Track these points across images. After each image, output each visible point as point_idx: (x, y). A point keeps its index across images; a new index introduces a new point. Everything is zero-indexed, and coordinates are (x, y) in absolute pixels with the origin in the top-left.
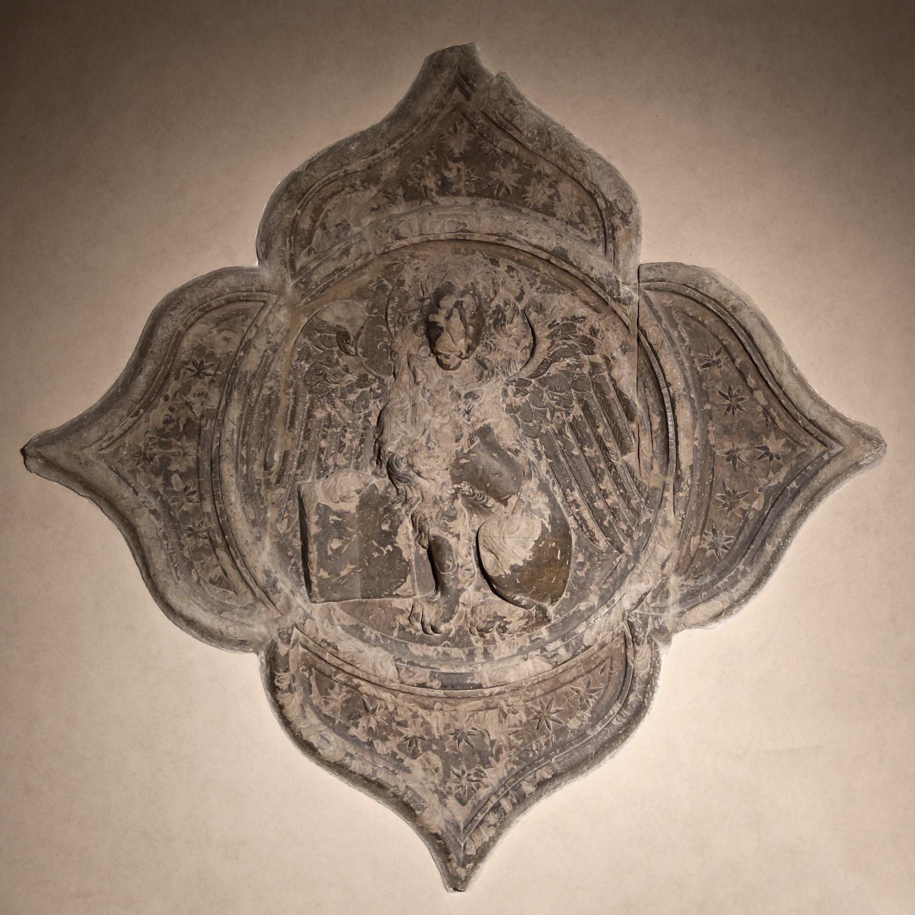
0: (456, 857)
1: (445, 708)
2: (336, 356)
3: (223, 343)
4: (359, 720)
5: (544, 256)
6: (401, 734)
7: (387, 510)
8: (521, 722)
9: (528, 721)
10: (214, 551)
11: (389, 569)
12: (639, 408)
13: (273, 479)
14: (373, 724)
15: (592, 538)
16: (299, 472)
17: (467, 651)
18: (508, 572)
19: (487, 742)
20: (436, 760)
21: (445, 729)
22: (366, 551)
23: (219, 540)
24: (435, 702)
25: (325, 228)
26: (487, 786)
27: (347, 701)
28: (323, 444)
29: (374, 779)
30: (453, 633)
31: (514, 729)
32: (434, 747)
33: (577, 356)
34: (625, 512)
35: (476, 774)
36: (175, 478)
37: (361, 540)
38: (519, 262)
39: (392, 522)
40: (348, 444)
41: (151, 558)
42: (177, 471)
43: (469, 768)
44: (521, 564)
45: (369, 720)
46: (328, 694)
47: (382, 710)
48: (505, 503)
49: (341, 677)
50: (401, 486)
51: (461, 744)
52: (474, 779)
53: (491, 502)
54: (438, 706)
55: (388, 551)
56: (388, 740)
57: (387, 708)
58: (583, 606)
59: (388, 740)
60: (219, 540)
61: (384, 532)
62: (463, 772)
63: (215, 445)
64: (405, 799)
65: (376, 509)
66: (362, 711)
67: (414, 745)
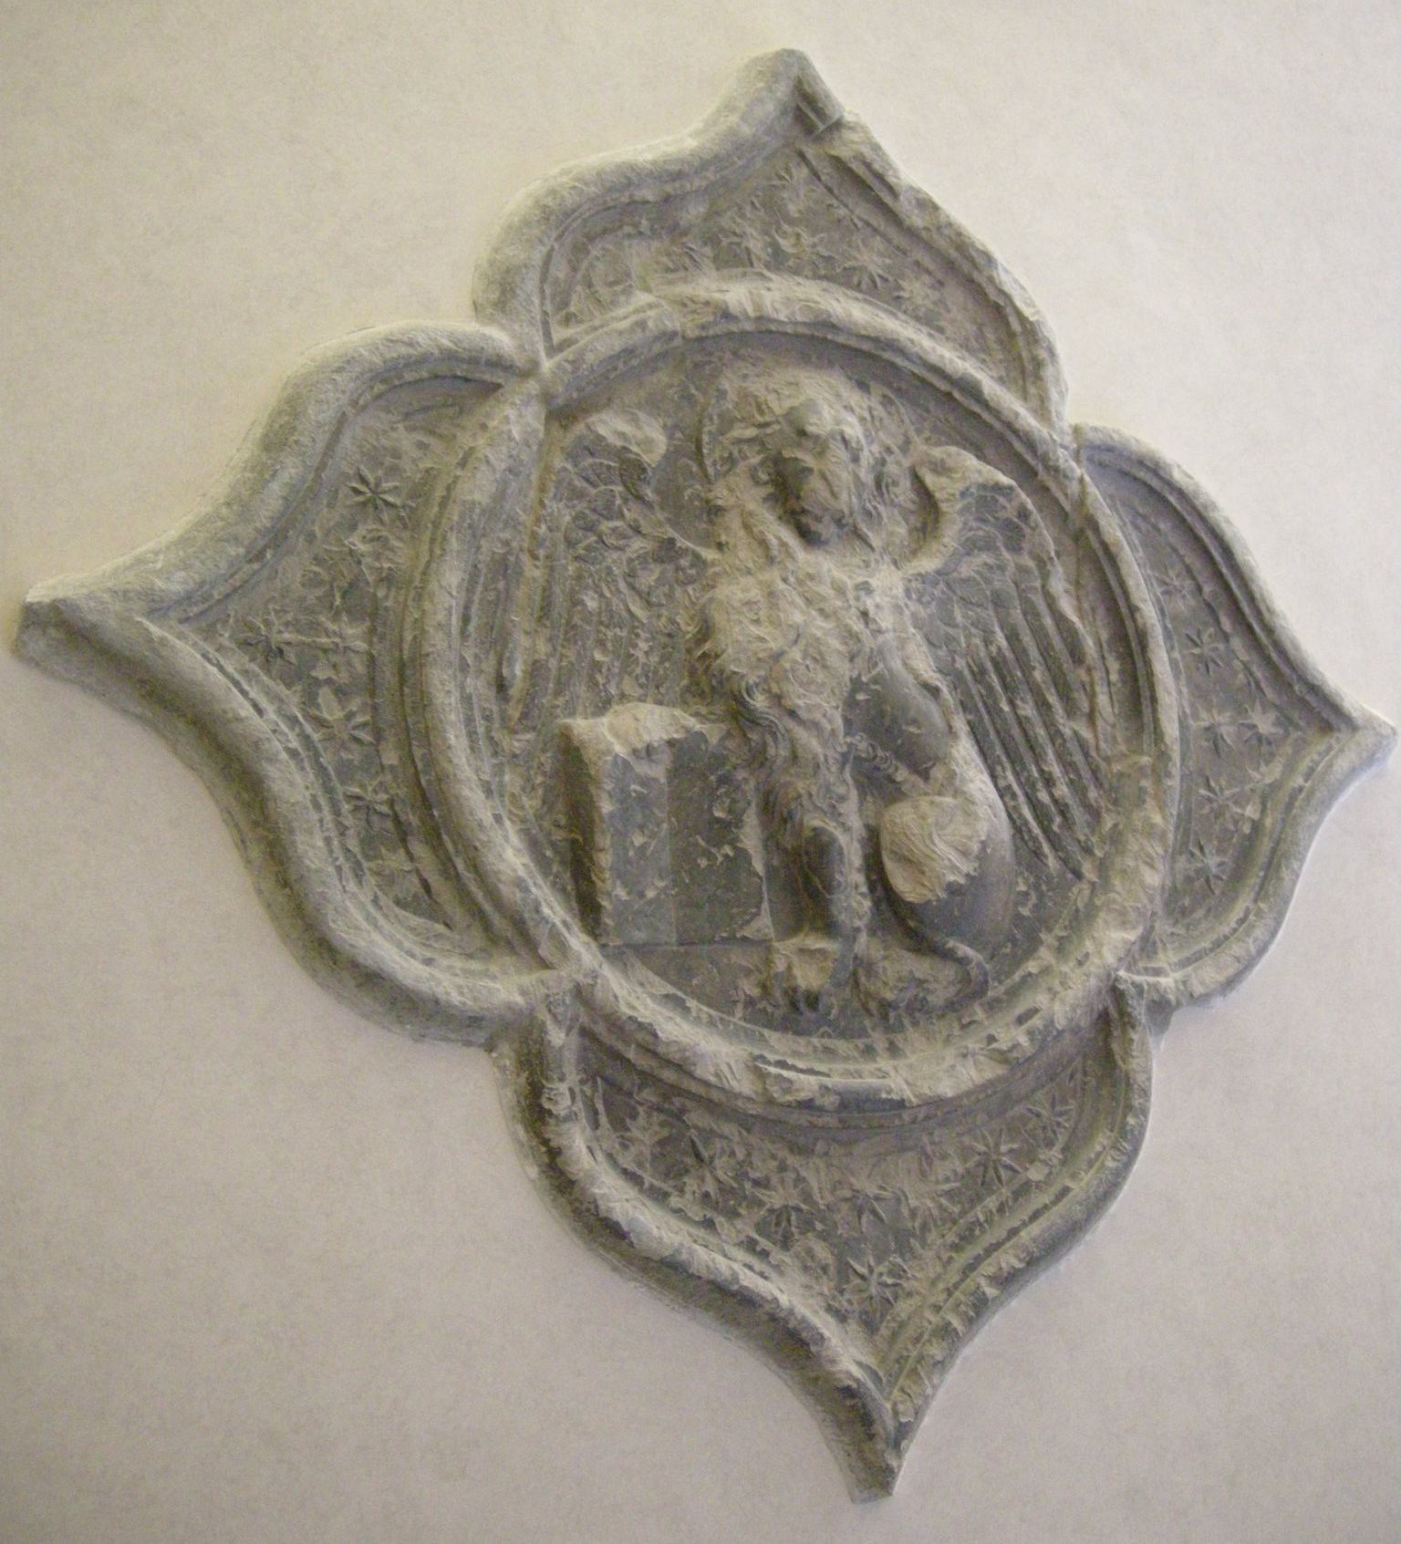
0: (864, 1435)
1: (832, 1152)
2: (618, 502)
3: (415, 453)
4: (686, 1179)
5: (943, 386)
6: (761, 1204)
7: (724, 780)
8: (955, 1173)
9: (968, 1171)
10: (404, 841)
11: (727, 888)
12: (1089, 644)
13: (515, 713)
14: (710, 1187)
15: (1037, 853)
16: (560, 701)
17: (861, 1046)
18: (943, 895)
19: (905, 1212)
20: (822, 1252)
21: (834, 1189)
22: (685, 856)
23: (413, 819)
24: (817, 1139)
25: (590, 285)
26: (910, 1295)
27: (661, 1143)
28: (598, 656)
29: (735, 1287)
30: (834, 1012)
31: (946, 1187)
32: (819, 1226)
33: (998, 555)
34: (1078, 813)
35: (891, 1273)
36: (325, 696)
37: (674, 834)
38: (898, 391)
39: (734, 801)
40: (642, 659)
41: (293, 842)
42: (329, 681)
43: (879, 1260)
44: (962, 881)
45: (703, 1179)
46: (628, 1129)
47: (725, 1159)
48: (925, 775)
49: (649, 1095)
50: (754, 736)
51: (864, 1219)
52: (890, 1281)
53: (902, 774)
54: (820, 1147)
55: (726, 856)
56: (738, 1215)
57: (733, 1154)
58: (1032, 966)
59: (738, 1215)
60: (413, 819)
61: (718, 820)
62: (871, 1270)
63: (408, 637)
64: (791, 1326)
65: (704, 777)
66: (690, 1161)
67: (784, 1224)
